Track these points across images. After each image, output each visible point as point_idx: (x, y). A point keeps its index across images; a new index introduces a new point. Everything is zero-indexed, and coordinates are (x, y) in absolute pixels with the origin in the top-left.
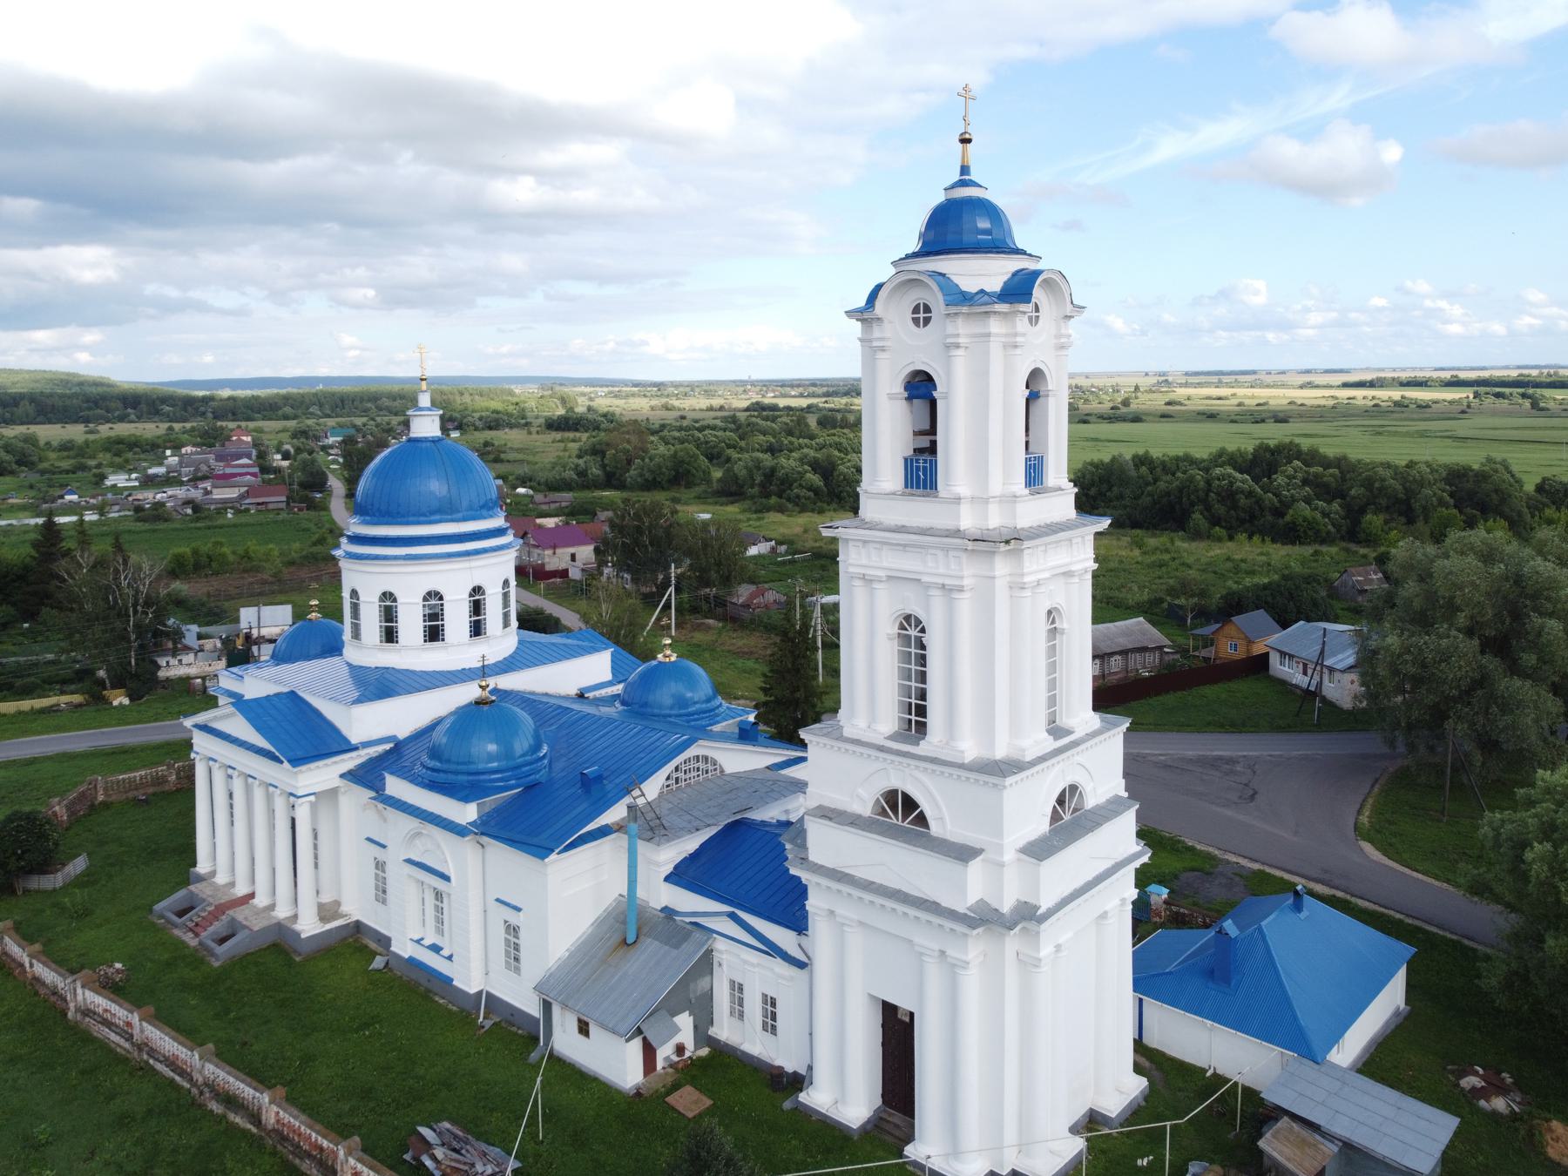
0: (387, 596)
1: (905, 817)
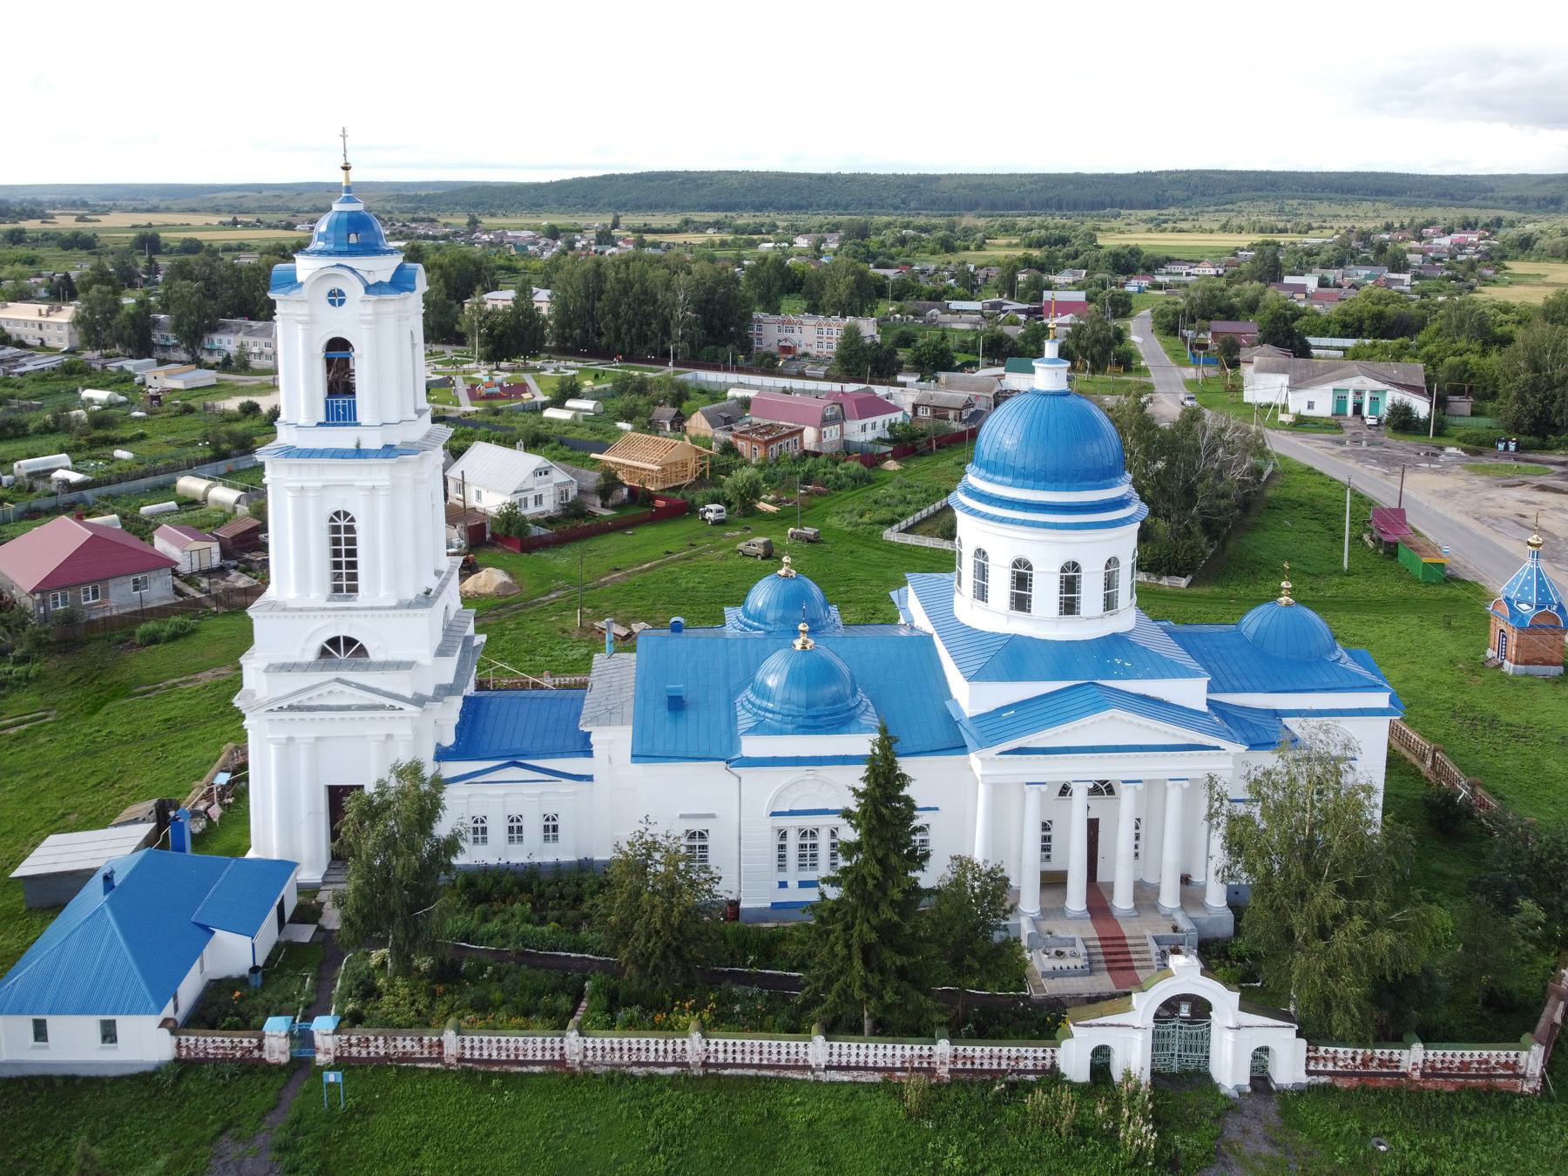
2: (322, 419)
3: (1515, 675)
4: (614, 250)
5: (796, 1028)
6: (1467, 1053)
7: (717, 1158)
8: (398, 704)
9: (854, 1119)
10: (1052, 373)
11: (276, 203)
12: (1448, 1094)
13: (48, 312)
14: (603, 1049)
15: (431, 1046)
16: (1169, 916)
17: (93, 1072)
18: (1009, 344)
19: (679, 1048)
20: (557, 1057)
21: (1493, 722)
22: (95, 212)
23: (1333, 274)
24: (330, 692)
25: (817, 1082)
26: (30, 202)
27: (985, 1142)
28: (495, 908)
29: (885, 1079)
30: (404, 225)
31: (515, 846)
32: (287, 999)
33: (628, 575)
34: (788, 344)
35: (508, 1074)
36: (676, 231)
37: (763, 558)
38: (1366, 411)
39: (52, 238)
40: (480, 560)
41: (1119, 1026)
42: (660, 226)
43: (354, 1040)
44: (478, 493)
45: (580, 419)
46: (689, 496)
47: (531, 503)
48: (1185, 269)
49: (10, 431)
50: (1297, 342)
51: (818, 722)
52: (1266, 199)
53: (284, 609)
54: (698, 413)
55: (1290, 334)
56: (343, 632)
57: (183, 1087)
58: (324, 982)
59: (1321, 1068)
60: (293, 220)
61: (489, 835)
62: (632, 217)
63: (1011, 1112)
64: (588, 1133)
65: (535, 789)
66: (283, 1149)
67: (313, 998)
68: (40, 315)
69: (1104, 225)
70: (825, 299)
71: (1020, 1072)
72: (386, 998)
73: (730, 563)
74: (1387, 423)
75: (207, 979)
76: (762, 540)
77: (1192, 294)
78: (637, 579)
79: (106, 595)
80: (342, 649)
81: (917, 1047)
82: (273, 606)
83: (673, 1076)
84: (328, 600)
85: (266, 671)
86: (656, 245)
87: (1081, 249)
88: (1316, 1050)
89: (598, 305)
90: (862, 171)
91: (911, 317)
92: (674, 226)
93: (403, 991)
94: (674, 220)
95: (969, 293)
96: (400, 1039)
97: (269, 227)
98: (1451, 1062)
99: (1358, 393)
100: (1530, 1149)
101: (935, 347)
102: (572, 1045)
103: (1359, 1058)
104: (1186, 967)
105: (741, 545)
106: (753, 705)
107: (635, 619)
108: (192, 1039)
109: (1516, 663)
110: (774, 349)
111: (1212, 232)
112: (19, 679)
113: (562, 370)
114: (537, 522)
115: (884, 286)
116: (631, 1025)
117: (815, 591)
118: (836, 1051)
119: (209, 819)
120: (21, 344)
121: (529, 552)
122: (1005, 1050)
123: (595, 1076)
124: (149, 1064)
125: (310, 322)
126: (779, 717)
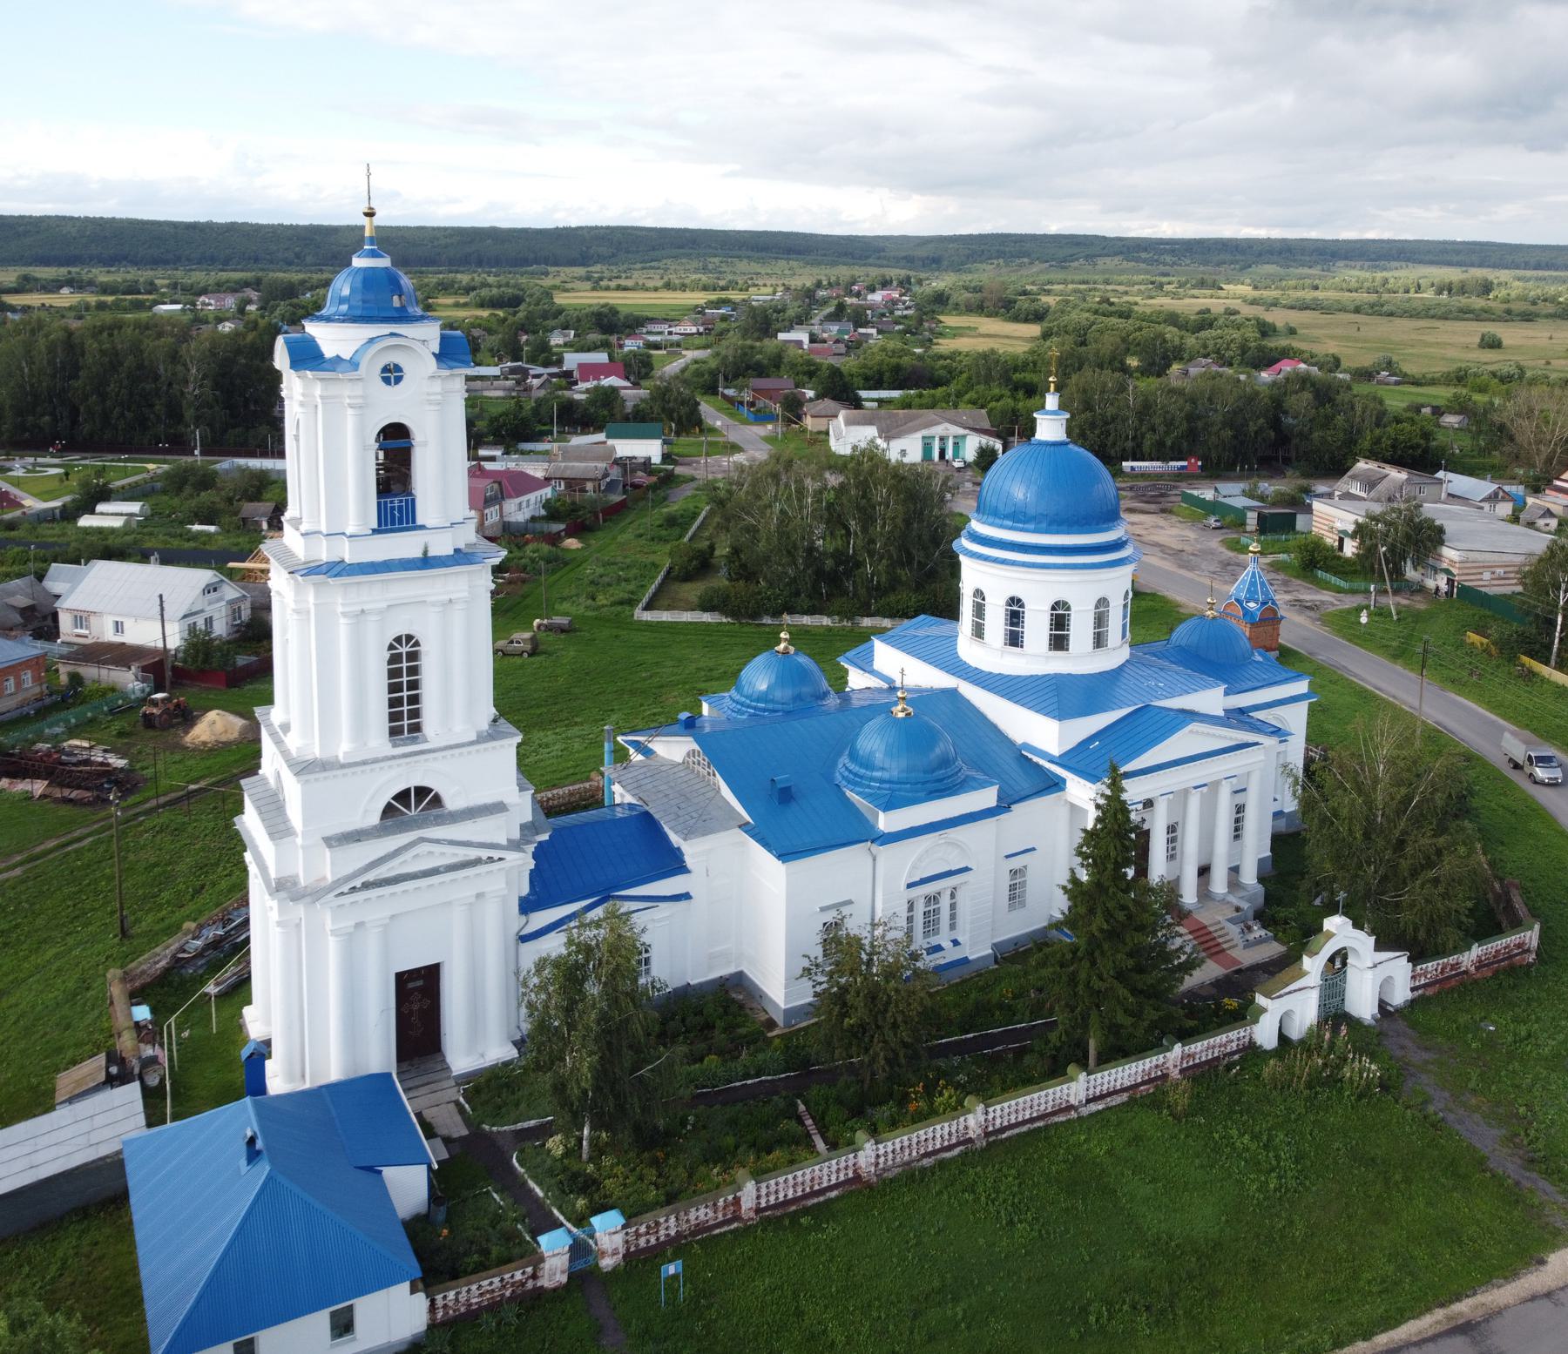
0: (1014, 601)
8: (496, 854)
29: (1130, 1097)
37: (530, 655)
38: (949, 455)
41: (1300, 990)
45: (134, 525)
48: (665, 328)
52: (688, 256)
64: (939, 1231)
77: (724, 352)
101: (516, 417)
111: (656, 289)
123: (891, 1181)
124: (401, 1343)
125: (361, 407)
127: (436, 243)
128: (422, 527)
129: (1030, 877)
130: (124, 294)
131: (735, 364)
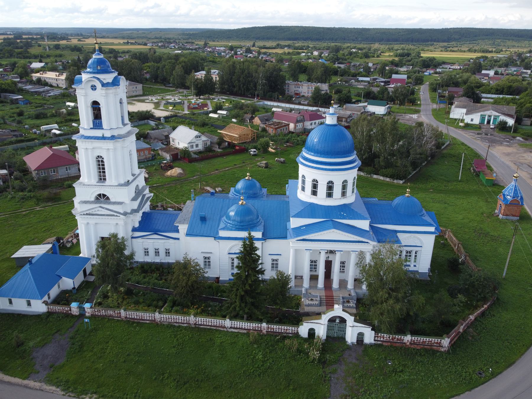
1: (103, 198)
2: (92, 127)
3: (502, 219)
4: (251, 55)
5: (224, 317)
6: (425, 339)
7: (192, 350)
8: (118, 215)
9: (235, 343)
10: (331, 118)
11: (144, 35)
12: (418, 349)
13: (59, 75)
14: (166, 318)
15: (118, 314)
16: (350, 291)
17: (26, 313)
18: (373, 94)
19: (188, 319)
20: (153, 319)
21: (487, 235)
22: (84, 38)
23: (500, 70)
24: (98, 210)
25: (228, 331)
26: (64, 34)
27: (271, 352)
28: (148, 275)
30: (183, 45)
31: (157, 257)
32: (82, 297)
33: (220, 172)
34: (298, 92)
35: (139, 322)
36: (274, 48)
39: (68, 48)
40: (174, 165)
41: (317, 323)
42: (269, 46)
43: (96, 310)
44: (179, 143)
45: (221, 117)
46: (247, 146)
47: (194, 147)
49: (42, 116)
50: (475, 96)
51: (243, 227)
53: (84, 185)
54: (257, 117)
55: (474, 93)
56: (102, 192)
57: (48, 319)
58: (94, 292)
59: (379, 339)
60: (147, 42)
61: (149, 253)
62: (261, 42)
63: (281, 345)
65: (163, 241)
66: (72, 338)
67: (90, 297)
68: (56, 76)
69: (426, 48)
70: (313, 77)
71: (287, 333)
72: (110, 299)
73: (254, 169)
74: (497, 127)
75: (61, 290)
76: (265, 162)
78: (222, 173)
79: (57, 172)
80: (102, 198)
81: (257, 324)
82: (81, 183)
83: (186, 327)
84: (97, 183)
85: (79, 203)
86: (265, 53)
87: (413, 58)
88: (378, 334)
89: (234, 77)
90: (343, 27)
91: (344, 83)
92: (274, 46)
93: (115, 297)
94: (274, 44)
95: (367, 74)
96: (109, 311)
97: (139, 44)
98: (420, 341)
99: (490, 116)
100: (436, 367)
102: (157, 316)
103: (391, 338)
104: (338, 308)
105: (258, 164)
106: (226, 222)
107: (218, 187)
108: (52, 307)
109: (503, 215)
110: (293, 94)
111: (464, 52)
112: (28, 197)
113: (220, 99)
114: (195, 153)
115: (338, 71)
116: (177, 312)
117: (258, 184)
118: (233, 323)
119: (73, 243)
120: (51, 86)
121: (191, 163)
122: (283, 327)
123: (164, 325)
124: (40, 312)
125: (86, 95)
126: (231, 225)
127: (399, 34)
128: (103, 129)
129: (279, 262)
130: (300, 50)
131: (447, 82)
